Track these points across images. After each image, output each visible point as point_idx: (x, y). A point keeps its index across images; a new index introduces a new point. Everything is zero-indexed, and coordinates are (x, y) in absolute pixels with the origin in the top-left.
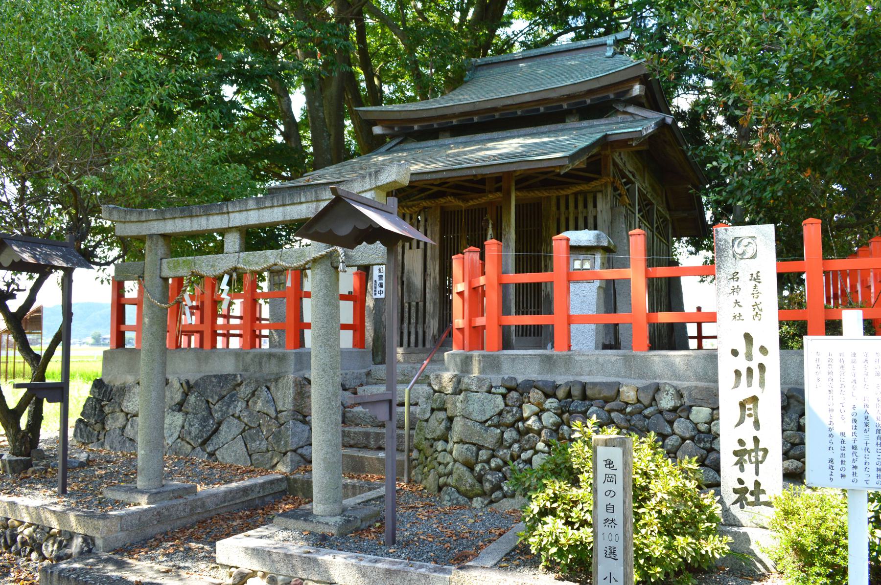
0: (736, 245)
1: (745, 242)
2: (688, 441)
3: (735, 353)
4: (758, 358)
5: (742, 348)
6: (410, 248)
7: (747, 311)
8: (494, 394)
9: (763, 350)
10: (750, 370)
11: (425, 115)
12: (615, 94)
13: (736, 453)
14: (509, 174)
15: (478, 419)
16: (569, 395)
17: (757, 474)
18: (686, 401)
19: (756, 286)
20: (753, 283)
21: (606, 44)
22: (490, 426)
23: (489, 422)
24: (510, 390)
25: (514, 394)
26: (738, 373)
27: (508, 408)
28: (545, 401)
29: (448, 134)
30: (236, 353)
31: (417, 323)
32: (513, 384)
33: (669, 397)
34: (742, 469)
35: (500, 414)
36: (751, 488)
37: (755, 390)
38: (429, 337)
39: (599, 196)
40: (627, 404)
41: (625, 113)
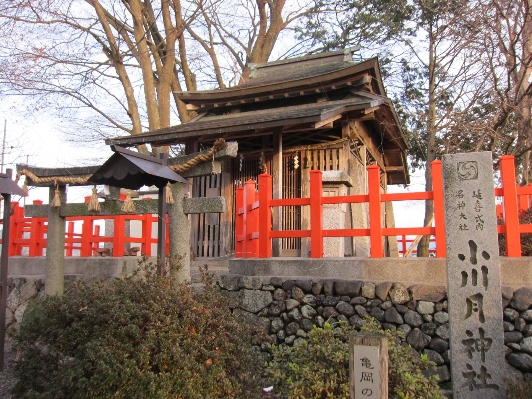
0: (460, 169)
1: (468, 166)
2: (416, 329)
3: (462, 257)
4: (481, 261)
5: (468, 253)
6: (210, 187)
7: (471, 224)
8: (264, 291)
9: (486, 255)
10: (474, 272)
11: (221, 97)
12: (352, 82)
13: (464, 342)
14: (277, 130)
15: (252, 310)
16: (323, 291)
17: (483, 360)
18: (415, 297)
19: (478, 201)
20: (476, 199)
21: (343, 54)
22: (261, 316)
23: (261, 313)
24: (277, 287)
25: (280, 291)
26: (464, 274)
27: (276, 302)
28: (303, 297)
29: (238, 111)
30: (77, 260)
31: (214, 239)
32: (280, 283)
33: (400, 294)
34: (471, 357)
35: (269, 306)
36: (478, 371)
37: (480, 288)
38: (222, 250)
39: (341, 151)
40: (367, 299)
41: (358, 96)
